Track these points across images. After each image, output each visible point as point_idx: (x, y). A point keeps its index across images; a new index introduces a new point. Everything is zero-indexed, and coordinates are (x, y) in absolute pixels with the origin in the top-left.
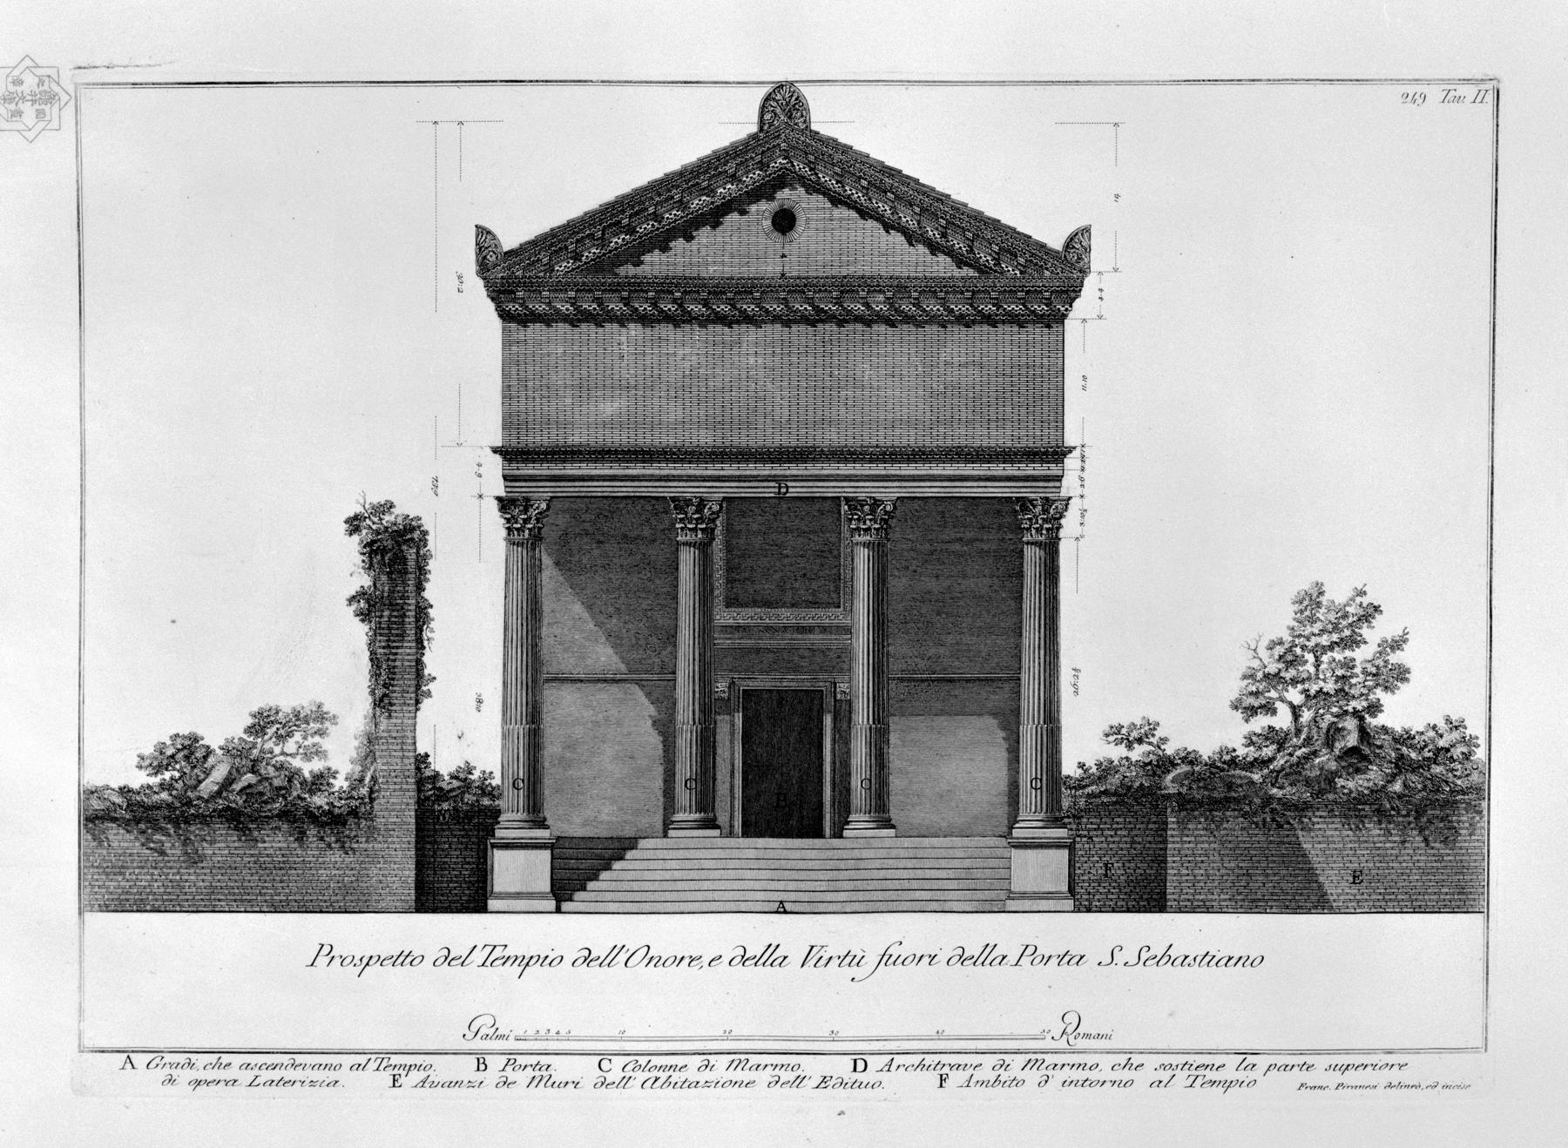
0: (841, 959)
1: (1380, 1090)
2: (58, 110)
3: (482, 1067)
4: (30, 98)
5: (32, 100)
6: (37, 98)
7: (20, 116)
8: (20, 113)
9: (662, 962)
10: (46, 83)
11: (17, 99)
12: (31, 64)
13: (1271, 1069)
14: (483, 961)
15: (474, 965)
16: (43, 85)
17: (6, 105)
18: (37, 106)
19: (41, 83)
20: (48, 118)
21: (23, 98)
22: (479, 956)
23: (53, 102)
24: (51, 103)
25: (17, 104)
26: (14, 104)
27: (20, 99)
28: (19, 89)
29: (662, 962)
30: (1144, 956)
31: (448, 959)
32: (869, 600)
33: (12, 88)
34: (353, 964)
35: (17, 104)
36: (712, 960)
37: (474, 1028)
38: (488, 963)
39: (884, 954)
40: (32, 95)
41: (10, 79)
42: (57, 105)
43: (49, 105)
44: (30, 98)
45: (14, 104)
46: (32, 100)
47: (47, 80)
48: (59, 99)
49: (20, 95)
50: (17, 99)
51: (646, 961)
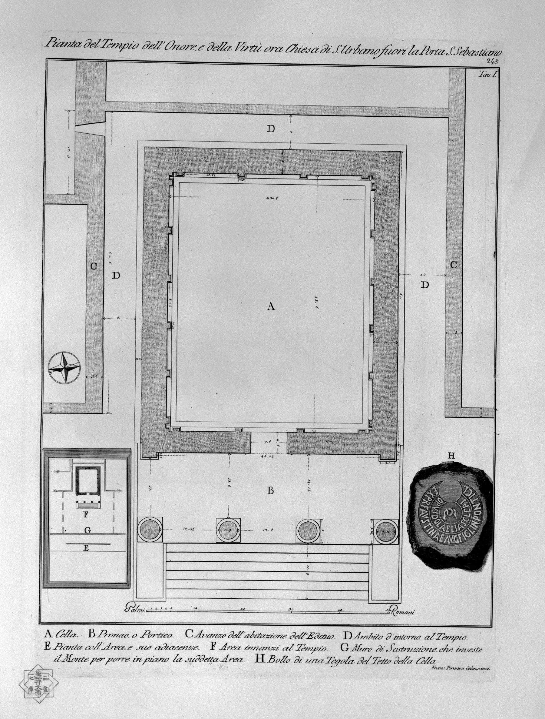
0: (355, 50)
1: (260, 663)
2: (43, 670)
3: (271, 492)
4: (38, 683)
5: (39, 682)
6: (38, 680)
7: (47, 687)
8: (45, 688)
9: (179, 47)
10: (32, 676)
11: (39, 689)
12: (22, 684)
13: (110, 660)
14: (47, 44)
15: (99, 48)
16: (32, 678)
17: (42, 694)
18: (42, 680)
19: (31, 678)
20: (47, 675)
21: (38, 686)
22: (101, 44)
23: (40, 673)
24: (40, 674)
25: (41, 689)
26: (41, 690)
27: (38, 688)
28: (34, 688)
29: (179, 47)
30: (460, 51)
31: (90, 45)
32: (88, 463)
33: (34, 691)
34: (337, 52)
35: (41, 689)
36: (200, 47)
37: (128, 606)
38: (105, 46)
39: (385, 49)
40: (37, 682)
41: (30, 693)
42: (41, 671)
43: (41, 674)
44: (38, 683)
45: (41, 690)
46: (39, 682)
47: (30, 676)
48: (38, 670)
49: (37, 688)
50: (39, 689)
51: (173, 47)
